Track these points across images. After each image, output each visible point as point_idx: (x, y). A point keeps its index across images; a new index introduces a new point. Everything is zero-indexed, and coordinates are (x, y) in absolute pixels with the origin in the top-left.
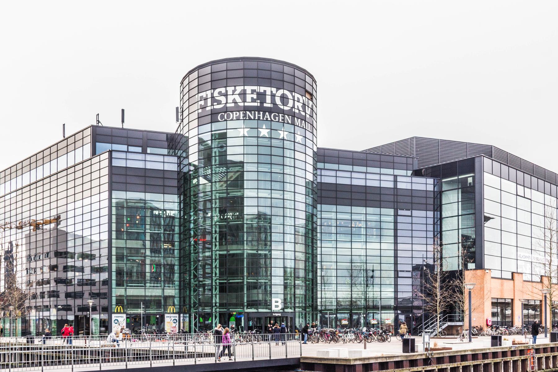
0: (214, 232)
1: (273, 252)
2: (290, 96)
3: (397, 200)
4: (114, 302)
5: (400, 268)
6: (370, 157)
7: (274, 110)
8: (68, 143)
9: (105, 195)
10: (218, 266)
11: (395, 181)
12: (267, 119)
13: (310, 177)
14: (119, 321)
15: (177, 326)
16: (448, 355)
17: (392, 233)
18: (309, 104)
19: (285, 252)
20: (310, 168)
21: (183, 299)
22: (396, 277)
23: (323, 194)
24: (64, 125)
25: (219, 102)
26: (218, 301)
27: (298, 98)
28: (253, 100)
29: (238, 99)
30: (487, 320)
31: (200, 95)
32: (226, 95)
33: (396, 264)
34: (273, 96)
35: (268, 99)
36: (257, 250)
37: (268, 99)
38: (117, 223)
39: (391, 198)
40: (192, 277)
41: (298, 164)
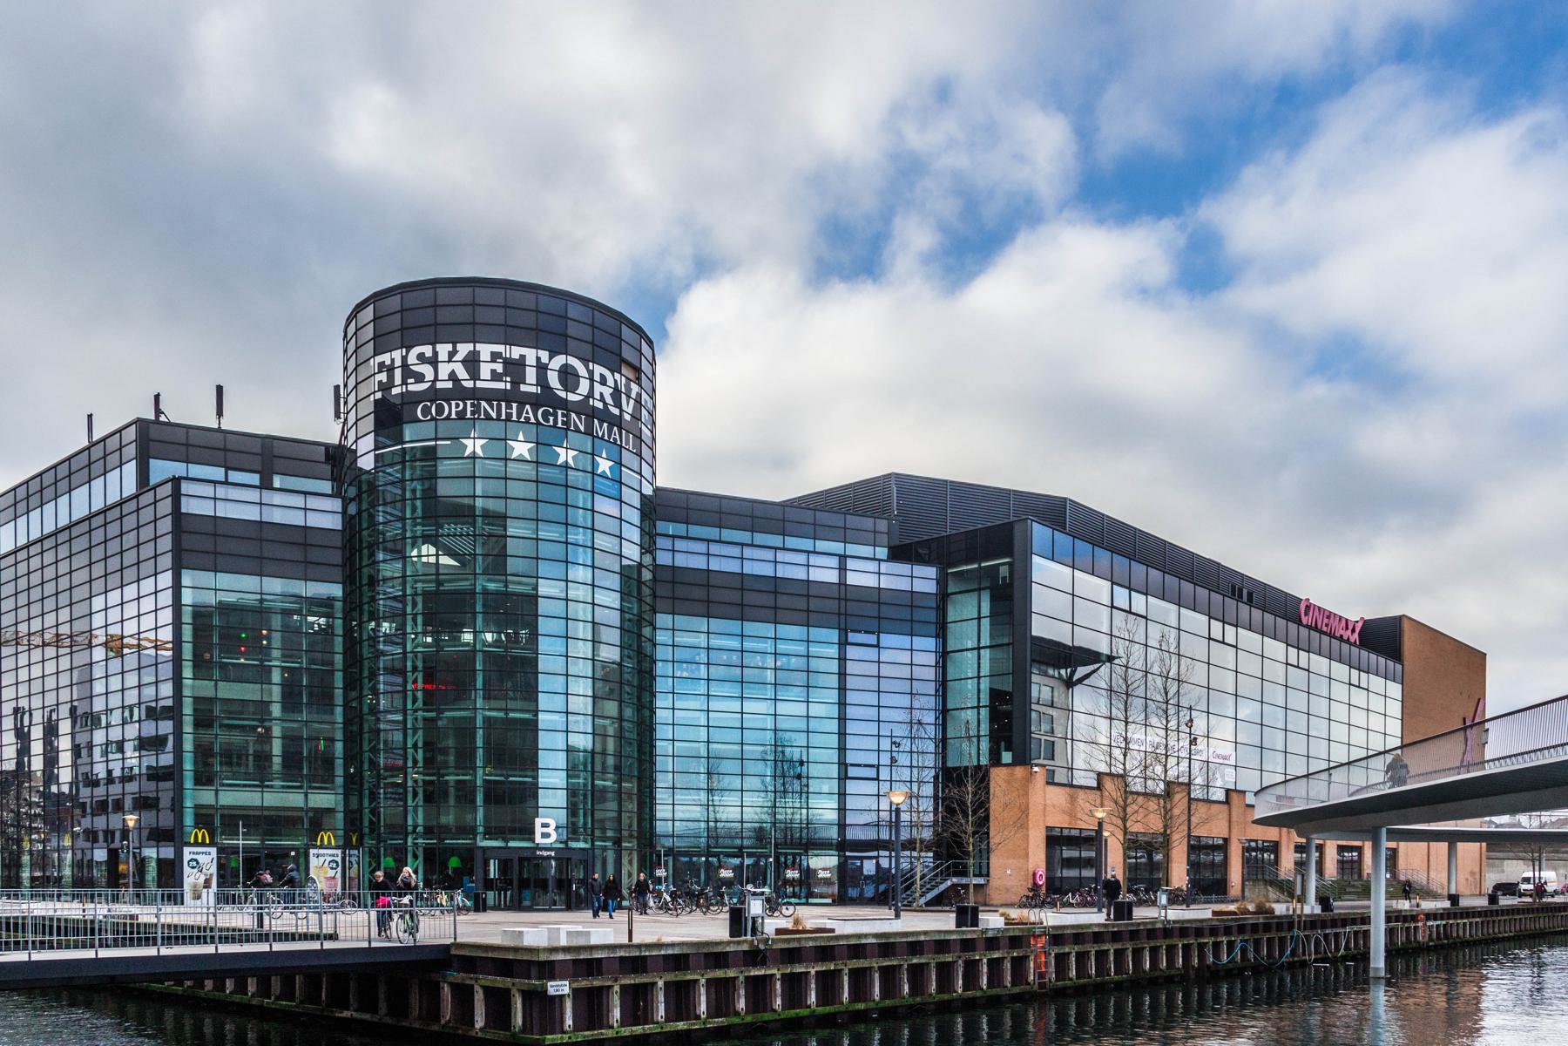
0: (409, 668)
1: (541, 716)
2: (582, 371)
3: (851, 613)
4: (189, 820)
5: (851, 758)
6: (792, 514)
7: (546, 399)
8: (89, 462)
9: (166, 579)
10: (420, 744)
11: (842, 569)
12: (527, 419)
13: (632, 552)
14: (199, 864)
15: (339, 875)
16: (811, 944)
17: (833, 681)
18: (629, 389)
19: (780, 734)
20: (634, 534)
21: (353, 821)
22: (843, 778)
23: (651, 594)
24: (90, 416)
25: (420, 378)
26: (420, 821)
27: (603, 377)
28: (495, 376)
29: (462, 373)
30: (1034, 875)
31: (379, 359)
32: (434, 362)
33: (842, 749)
34: (542, 368)
35: (531, 375)
36: (506, 710)
37: (531, 375)
38: (195, 643)
39: (833, 605)
40: (366, 766)
41: (600, 522)
